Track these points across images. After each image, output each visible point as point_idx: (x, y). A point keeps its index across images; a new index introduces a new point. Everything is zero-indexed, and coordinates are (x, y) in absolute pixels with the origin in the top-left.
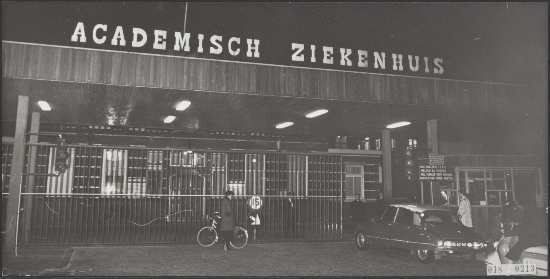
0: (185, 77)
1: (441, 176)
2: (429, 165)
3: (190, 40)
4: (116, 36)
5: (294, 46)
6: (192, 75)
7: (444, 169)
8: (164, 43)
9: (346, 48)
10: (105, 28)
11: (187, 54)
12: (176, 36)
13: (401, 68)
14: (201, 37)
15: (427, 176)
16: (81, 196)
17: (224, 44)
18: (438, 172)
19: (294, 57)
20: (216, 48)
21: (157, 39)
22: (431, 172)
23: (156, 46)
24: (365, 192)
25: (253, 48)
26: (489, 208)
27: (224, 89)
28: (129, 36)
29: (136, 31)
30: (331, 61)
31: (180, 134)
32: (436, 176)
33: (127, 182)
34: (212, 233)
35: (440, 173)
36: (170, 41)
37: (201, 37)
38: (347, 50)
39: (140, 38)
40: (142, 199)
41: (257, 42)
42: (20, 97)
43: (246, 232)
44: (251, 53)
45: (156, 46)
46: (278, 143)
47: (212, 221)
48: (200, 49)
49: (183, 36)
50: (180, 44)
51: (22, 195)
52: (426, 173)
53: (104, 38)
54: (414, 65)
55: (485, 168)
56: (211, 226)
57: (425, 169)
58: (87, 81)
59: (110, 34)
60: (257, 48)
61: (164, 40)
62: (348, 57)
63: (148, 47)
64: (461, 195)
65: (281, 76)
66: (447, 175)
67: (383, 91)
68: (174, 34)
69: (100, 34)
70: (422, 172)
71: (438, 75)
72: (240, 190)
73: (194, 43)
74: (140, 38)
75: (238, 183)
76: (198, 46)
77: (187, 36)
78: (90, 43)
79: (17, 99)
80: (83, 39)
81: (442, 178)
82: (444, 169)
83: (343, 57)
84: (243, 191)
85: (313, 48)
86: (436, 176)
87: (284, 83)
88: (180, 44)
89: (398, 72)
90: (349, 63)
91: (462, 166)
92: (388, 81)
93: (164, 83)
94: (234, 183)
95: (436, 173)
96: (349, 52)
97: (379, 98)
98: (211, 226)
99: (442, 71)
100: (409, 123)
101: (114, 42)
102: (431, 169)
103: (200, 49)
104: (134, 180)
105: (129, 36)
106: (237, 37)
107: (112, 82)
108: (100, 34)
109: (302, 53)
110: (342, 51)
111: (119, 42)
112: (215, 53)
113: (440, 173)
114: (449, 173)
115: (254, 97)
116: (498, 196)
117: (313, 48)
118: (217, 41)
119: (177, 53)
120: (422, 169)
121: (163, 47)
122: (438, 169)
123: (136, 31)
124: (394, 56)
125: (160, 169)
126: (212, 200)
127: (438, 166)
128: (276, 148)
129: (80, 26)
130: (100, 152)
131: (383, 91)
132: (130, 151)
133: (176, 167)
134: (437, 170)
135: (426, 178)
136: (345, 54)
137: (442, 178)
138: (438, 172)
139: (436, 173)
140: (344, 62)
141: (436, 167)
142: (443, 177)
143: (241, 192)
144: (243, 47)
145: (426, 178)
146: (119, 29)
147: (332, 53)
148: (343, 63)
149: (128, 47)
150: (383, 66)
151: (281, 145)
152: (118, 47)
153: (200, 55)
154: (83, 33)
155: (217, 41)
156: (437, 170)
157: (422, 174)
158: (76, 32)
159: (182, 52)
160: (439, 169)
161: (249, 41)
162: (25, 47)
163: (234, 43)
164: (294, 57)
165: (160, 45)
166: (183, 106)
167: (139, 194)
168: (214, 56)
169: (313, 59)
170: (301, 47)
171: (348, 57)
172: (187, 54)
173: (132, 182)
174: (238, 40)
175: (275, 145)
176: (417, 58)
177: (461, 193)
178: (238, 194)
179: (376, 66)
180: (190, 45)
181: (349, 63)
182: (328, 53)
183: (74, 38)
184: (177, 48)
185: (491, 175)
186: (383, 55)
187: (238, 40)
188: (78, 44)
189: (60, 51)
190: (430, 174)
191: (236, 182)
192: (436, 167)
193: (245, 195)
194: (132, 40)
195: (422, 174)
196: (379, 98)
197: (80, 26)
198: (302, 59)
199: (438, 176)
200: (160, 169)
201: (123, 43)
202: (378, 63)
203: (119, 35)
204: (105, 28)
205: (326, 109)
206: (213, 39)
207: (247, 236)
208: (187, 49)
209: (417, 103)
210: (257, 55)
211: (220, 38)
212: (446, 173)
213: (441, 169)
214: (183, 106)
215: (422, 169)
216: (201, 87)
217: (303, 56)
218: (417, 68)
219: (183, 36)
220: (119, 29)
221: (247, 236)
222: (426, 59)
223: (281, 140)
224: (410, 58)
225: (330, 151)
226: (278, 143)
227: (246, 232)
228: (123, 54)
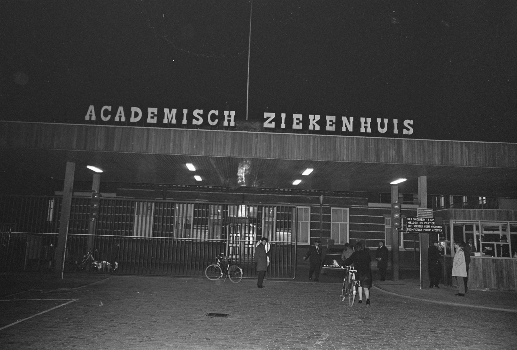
0: (171, 144)
1: (429, 228)
2: (417, 218)
3: (176, 114)
4: (118, 114)
5: (266, 115)
6: (177, 142)
7: (433, 222)
8: (156, 118)
10: (109, 108)
11: (173, 126)
12: (165, 111)
13: (369, 130)
15: (413, 228)
16: (83, 236)
17: (204, 116)
18: (426, 225)
19: (266, 125)
20: (408, 129)
21: (150, 115)
22: (419, 224)
23: (149, 120)
24: (311, 239)
25: (366, 125)
26: (483, 259)
27: (203, 154)
28: (128, 114)
29: (134, 109)
30: (333, 128)
31: (236, 191)
32: (423, 228)
33: (193, 229)
34: (217, 270)
35: (428, 225)
36: (161, 116)
37: (185, 111)
38: (316, 116)
39: (136, 115)
40: (150, 241)
41: (233, 113)
42: (68, 163)
43: (241, 270)
45: (149, 120)
46: (321, 198)
47: (217, 260)
48: (185, 122)
49: (170, 112)
50: (168, 118)
51: (68, 235)
52: (413, 225)
53: (109, 117)
54: (382, 126)
55: (509, 222)
56: (216, 264)
57: (413, 221)
58: (152, 151)
59: (113, 113)
60: (363, 125)
61: (333, 123)
62: (316, 122)
63: (143, 122)
64: (457, 246)
65: (253, 141)
67: (350, 152)
68: (341, 118)
69: (106, 113)
70: (409, 224)
71: (407, 136)
72: (286, 237)
73: (179, 117)
74: (136, 115)
75: (288, 232)
77: (174, 111)
78: (99, 120)
79: (66, 164)
80: (94, 118)
81: (430, 230)
82: (433, 222)
83: (312, 122)
84: (288, 238)
85: (283, 116)
86: (423, 228)
87: (256, 147)
88: (168, 118)
89: (366, 134)
91: (455, 219)
92: (296, 139)
93: (297, 155)
94: (280, 231)
95: (424, 225)
96: (318, 118)
97: (345, 158)
98: (216, 264)
99: (411, 131)
100: (89, 167)
101: (117, 119)
102: (419, 222)
103: (185, 122)
104: (199, 228)
105: (128, 114)
106: (109, 105)
107: (115, 149)
108: (106, 113)
110: (311, 117)
111: (120, 119)
113: (428, 225)
114: (439, 225)
115: (373, 164)
116: (493, 249)
118: (409, 124)
119: (165, 125)
120: (409, 221)
121: (300, 127)
122: (426, 221)
123: (134, 109)
124: (362, 120)
125: (220, 218)
126: (174, 242)
127: (426, 219)
128: (320, 203)
129: (92, 108)
130: (173, 205)
131: (350, 152)
132: (196, 205)
134: (425, 223)
135: (413, 230)
136: (314, 120)
137: (430, 230)
138: (426, 225)
139: (424, 225)
141: (424, 220)
142: (432, 229)
143: (286, 239)
144: (221, 118)
145: (413, 230)
146: (121, 109)
147: (334, 121)
148: (311, 127)
149: (128, 122)
150: (351, 129)
151: (324, 199)
152: (120, 123)
153: (283, 130)
154: (93, 113)
156: (425, 223)
157: (409, 226)
158: (89, 113)
159: (170, 125)
161: (226, 113)
162: (291, 136)
163: (106, 110)
164: (266, 125)
165: (152, 119)
166: (308, 172)
167: (203, 239)
168: (196, 126)
169: (283, 126)
170: (272, 115)
171: (316, 122)
172: (173, 126)
173: (197, 229)
174: (216, 113)
175: (318, 199)
176: (386, 121)
177: (457, 243)
178: (288, 240)
179: (344, 129)
180: (176, 118)
181: (318, 128)
182: (331, 121)
183: (87, 118)
184: (165, 121)
185: (509, 229)
186: (352, 119)
187: (216, 113)
188: (90, 122)
189: (230, 134)
191: (282, 230)
192: (424, 220)
193: (207, 239)
194: (131, 117)
195: (409, 226)
196: (345, 158)
197: (92, 108)
198: (273, 125)
199: (425, 228)
200: (220, 218)
201: (123, 119)
202: (346, 126)
203: (120, 113)
204: (109, 108)
205: (310, 168)
206: (406, 123)
207: (242, 273)
208: (174, 122)
209: (383, 161)
210: (232, 124)
211: (201, 112)
213: (430, 221)
214: (308, 172)
215: (409, 221)
216: (184, 152)
217: (273, 123)
218: (385, 130)
219: (170, 112)
220: (121, 109)
221: (242, 273)
222: (395, 121)
223: (324, 195)
224: (379, 120)
225: (370, 204)
226: (321, 198)
227: (241, 270)
228: (123, 128)
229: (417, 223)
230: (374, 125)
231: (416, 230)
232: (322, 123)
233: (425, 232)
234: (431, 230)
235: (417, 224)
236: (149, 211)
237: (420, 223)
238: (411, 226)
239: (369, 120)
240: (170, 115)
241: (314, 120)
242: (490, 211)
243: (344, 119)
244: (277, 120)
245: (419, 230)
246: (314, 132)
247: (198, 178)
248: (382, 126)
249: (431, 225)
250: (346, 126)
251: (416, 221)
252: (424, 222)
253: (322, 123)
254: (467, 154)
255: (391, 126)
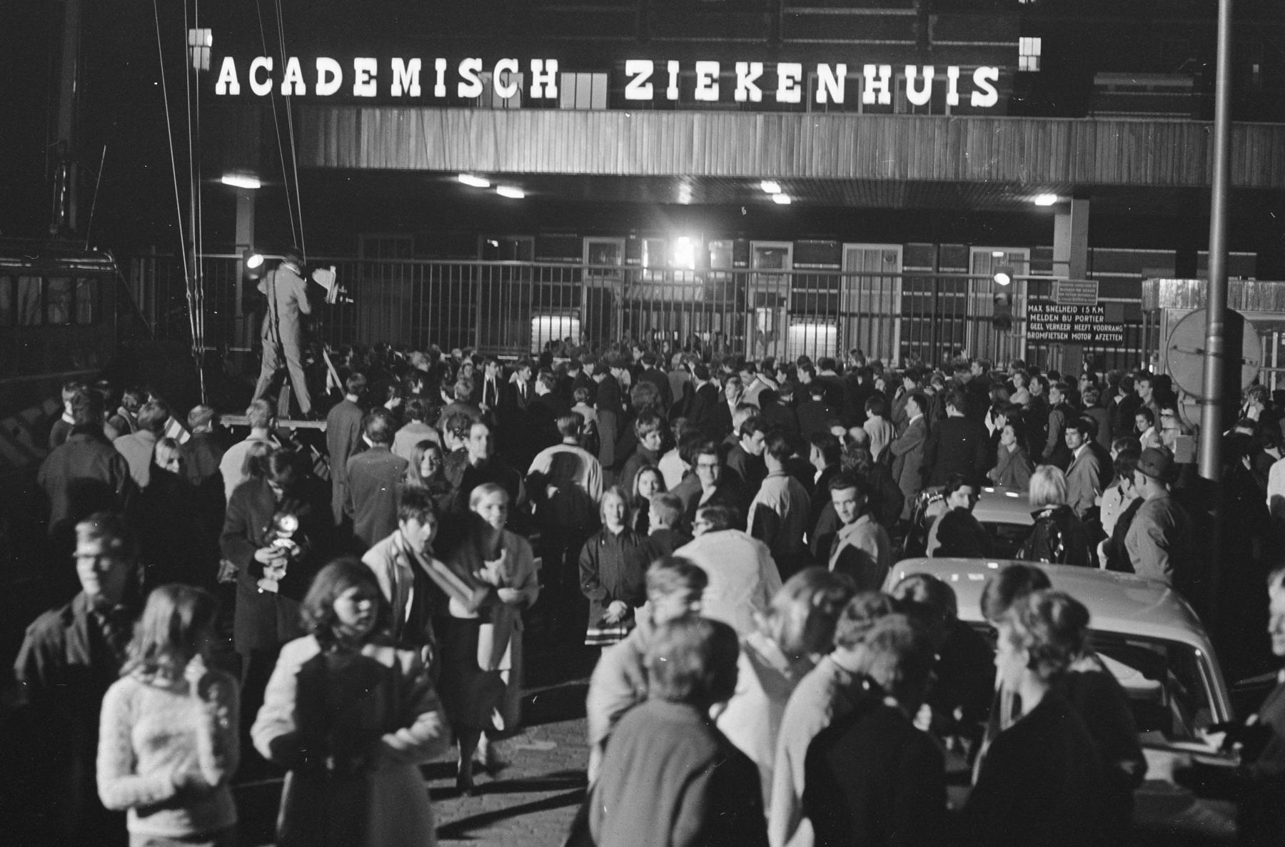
1: (1087, 332)
4: (288, 78)
9: (749, 59)
10: (268, 63)
13: (885, 98)
14: (441, 65)
15: (1045, 330)
18: (1078, 322)
22: (1060, 321)
28: (310, 76)
32: (1072, 331)
35: (1085, 323)
36: (384, 77)
37: (441, 65)
44: (873, 95)
52: (1044, 324)
54: (919, 86)
59: (277, 75)
62: (755, 82)
66: (1107, 328)
69: (262, 75)
73: (427, 77)
76: (435, 83)
77: (416, 64)
85: (673, 67)
86: (1072, 331)
90: (757, 95)
95: (1073, 323)
96: (758, 69)
100: (228, 180)
102: (1060, 315)
105: (310, 76)
108: (262, 75)
109: (648, 80)
112: (982, 104)
113: (1085, 323)
117: (673, 67)
118: (988, 80)
121: (713, 94)
122: (1079, 313)
133: (919, 297)
134: (1077, 318)
135: (1044, 335)
138: (1078, 322)
139: (1073, 323)
140: (745, 92)
142: (1094, 333)
146: (294, 64)
148: (740, 95)
150: (839, 97)
155: (988, 80)
160: (1084, 314)
165: (366, 86)
171: (755, 82)
176: (929, 72)
179: (821, 97)
180: (421, 83)
181: (757, 95)
190: (1056, 327)
192: (1075, 310)
202: (836, 79)
204: (268, 63)
208: (416, 91)
212: (1104, 323)
213: (1091, 313)
220: (294, 64)
229: (1056, 318)
230: (897, 85)
231: (1051, 336)
232: (768, 82)
233: (1076, 342)
234: (1093, 337)
235: (1056, 322)
236: (1106, 154)
237: (1064, 319)
238: (1039, 327)
239: (886, 71)
240: (406, 75)
241: (747, 75)
242: (518, 267)
243: (823, 70)
244: (659, 79)
245: (1060, 337)
246: (748, 106)
247: (890, 702)
248: (919, 86)
249: (1093, 323)
250: (836, 79)
251: (1054, 313)
252: (1074, 315)
253: (768, 82)
254: (1133, 151)
255: (940, 89)
